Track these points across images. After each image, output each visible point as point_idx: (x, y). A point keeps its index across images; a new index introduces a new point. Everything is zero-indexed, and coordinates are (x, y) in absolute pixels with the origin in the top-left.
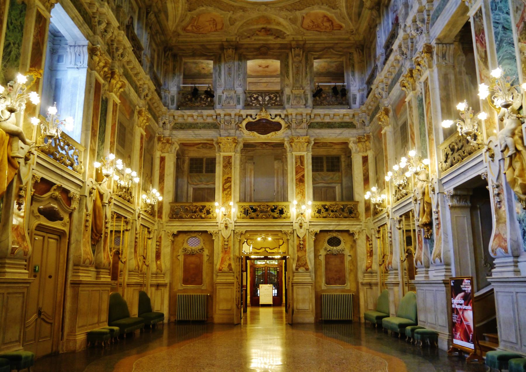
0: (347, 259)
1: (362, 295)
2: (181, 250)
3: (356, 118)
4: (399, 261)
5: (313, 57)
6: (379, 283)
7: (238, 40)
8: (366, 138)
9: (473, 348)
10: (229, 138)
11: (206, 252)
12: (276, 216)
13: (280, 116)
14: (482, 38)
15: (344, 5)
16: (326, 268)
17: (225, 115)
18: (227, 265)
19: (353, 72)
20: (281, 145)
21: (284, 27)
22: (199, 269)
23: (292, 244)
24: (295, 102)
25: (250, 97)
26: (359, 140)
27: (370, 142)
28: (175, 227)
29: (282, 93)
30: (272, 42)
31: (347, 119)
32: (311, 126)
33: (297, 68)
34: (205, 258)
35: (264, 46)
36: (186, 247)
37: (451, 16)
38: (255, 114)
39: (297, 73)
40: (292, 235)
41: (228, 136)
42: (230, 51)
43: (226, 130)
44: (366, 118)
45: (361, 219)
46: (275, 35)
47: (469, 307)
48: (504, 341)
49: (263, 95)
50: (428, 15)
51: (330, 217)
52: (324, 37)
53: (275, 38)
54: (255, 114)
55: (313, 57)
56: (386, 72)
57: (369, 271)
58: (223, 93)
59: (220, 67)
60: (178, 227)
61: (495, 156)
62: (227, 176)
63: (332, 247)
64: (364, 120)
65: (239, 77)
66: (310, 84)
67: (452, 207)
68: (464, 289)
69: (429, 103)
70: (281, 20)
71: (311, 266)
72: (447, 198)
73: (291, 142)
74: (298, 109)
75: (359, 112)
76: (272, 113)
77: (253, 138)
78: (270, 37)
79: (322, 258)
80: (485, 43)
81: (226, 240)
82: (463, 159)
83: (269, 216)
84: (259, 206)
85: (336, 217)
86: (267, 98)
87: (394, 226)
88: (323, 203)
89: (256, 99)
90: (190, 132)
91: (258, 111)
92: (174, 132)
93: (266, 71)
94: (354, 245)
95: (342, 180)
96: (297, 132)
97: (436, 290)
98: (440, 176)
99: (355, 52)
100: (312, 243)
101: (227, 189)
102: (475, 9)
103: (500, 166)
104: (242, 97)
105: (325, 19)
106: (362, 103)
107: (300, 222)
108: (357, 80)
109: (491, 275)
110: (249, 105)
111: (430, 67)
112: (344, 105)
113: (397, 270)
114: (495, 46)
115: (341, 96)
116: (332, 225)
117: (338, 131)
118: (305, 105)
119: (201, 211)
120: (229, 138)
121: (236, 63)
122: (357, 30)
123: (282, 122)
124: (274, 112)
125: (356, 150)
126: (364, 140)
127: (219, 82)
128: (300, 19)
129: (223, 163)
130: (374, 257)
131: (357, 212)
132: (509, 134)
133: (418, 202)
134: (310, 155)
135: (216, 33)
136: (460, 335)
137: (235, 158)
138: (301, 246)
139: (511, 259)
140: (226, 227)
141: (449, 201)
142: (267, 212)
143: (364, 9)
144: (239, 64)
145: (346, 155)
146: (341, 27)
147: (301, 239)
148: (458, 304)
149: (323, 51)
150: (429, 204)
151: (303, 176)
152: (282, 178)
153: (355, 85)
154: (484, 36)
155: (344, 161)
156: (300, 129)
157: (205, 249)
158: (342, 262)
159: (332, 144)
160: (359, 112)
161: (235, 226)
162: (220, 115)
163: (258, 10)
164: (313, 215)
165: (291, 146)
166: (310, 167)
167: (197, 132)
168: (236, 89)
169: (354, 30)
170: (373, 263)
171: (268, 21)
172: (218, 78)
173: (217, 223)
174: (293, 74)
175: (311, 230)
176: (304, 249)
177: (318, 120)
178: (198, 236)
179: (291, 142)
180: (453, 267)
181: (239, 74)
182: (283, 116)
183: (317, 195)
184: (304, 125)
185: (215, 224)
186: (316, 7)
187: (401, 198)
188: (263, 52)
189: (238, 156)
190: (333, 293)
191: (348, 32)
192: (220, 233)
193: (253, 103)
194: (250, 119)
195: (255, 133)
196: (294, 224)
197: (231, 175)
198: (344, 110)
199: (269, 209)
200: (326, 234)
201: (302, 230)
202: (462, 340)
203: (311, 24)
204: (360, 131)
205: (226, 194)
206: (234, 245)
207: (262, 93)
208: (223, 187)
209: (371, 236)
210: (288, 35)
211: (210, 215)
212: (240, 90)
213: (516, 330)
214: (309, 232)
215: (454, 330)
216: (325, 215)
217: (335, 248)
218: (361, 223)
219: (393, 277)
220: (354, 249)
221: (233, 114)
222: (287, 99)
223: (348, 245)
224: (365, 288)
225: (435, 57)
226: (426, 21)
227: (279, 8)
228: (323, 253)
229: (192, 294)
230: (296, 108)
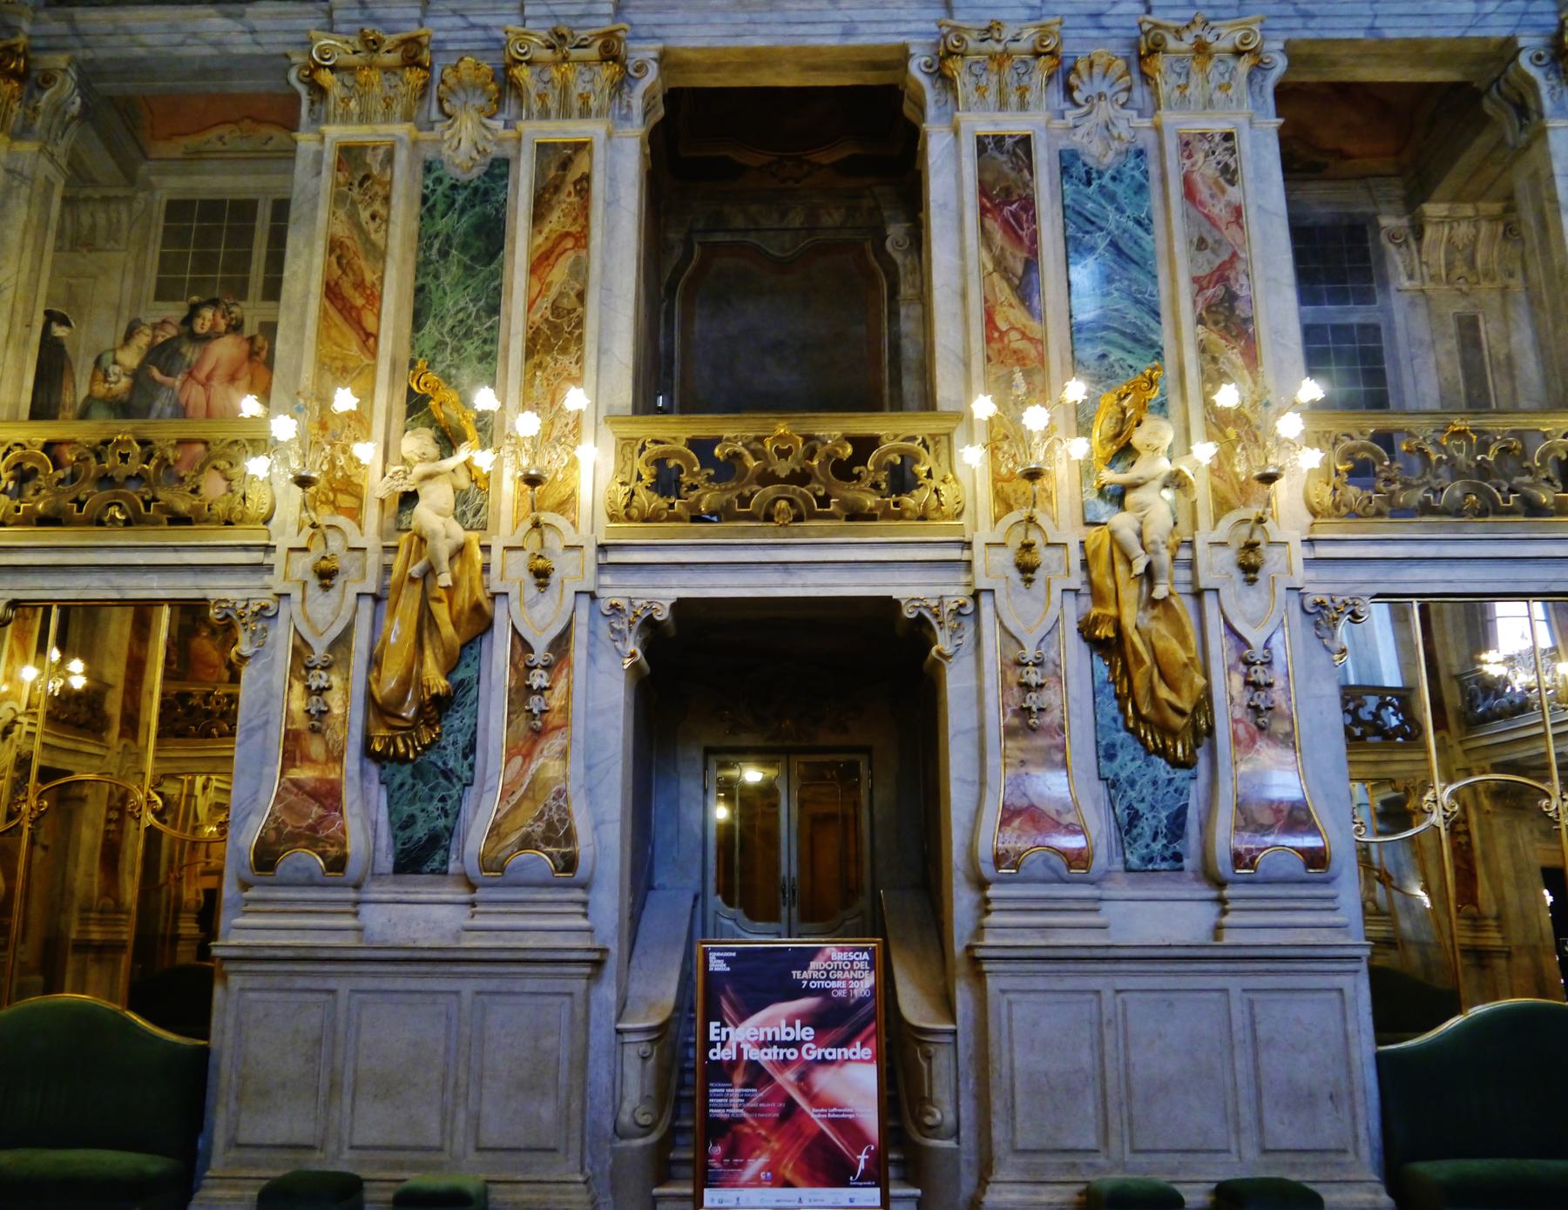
51: (751, 517)
68: (814, 985)
82: (798, 518)
98: (579, 271)
133: (124, 430)
136: (771, 1167)
140: (542, 576)
164: (621, 500)
196: (978, 555)
202: (788, 1184)
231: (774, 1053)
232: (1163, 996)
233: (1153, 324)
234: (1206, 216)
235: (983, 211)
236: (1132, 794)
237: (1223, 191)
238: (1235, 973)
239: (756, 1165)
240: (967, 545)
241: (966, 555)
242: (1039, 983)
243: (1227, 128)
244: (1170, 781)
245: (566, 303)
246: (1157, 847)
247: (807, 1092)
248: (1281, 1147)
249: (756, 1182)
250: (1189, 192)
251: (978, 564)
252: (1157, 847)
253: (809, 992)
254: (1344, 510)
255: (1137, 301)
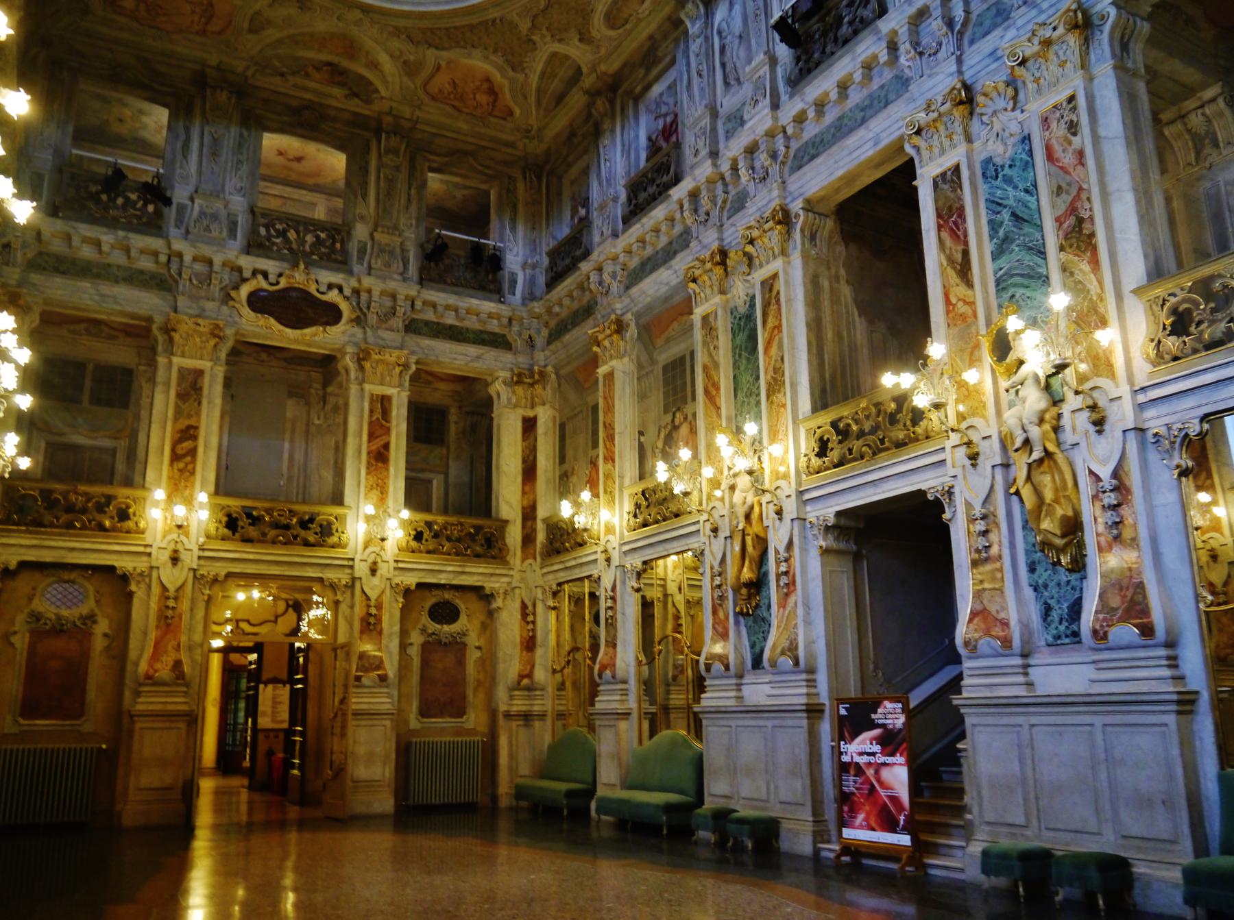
0: (473, 656)
1: (503, 741)
2: (21, 618)
3: (516, 328)
4: (633, 662)
5: (427, 164)
6: (549, 714)
7: (249, 73)
8: (536, 377)
9: (909, 844)
10: (200, 321)
11: (102, 626)
12: (312, 539)
13: (340, 289)
14: (955, 223)
15: (540, 68)
16: (422, 678)
17: (195, 259)
18: (171, 663)
19: (513, 221)
20: (327, 364)
21: (383, 76)
22: (76, 671)
23: (348, 612)
24: (379, 262)
25: (267, 226)
26: (518, 379)
27: (544, 388)
28: (13, 550)
29: (349, 233)
30: (334, 103)
31: (494, 326)
32: (412, 327)
33: (391, 181)
34: (99, 643)
35: (309, 106)
36: (41, 609)
37: (855, 163)
38: (274, 272)
39: (389, 194)
40: (349, 593)
41: (198, 316)
42: (223, 96)
43: (194, 298)
44: (539, 332)
45: (512, 562)
46: (350, 89)
47: (899, 759)
48: (988, 823)
49: (301, 228)
50: (787, 147)
51: (855, 459)
52: (463, 125)
53: (346, 96)
54: (277, 271)
55: (427, 164)
56: (633, 240)
57: (525, 683)
58: (192, 199)
59: (187, 130)
60: (23, 551)
61: (981, 458)
62: (187, 422)
63: (438, 626)
64: (534, 335)
65: (238, 169)
66: (417, 227)
67: (825, 552)
68: (880, 722)
69: (779, 327)
70: (383, 58)
71: (391, 669)
72: (816, 531)
73: (362, 357)
74: (388, 282)
75: (525, 315)
76: (321, 279)
77: (263, 331)
78: (337, 92)
79: (414, 652)
80: (966, 236)
81: (172, 593)
82: (874, 454)
83: (295, 537)
84: (269, 511)
85: (457, 554)
86: (309, 238)
87: (624, 582)
88: (429, 518)
89: (282, 234)
90: (85, 285)
91: (286, 265)
92: (35, 277)
93: (290, 169)
94: (488, 621)
95: (447, 466)
96: (380, 337)
97: (774, 727)
98: (799, 483)
99: (520, 178)
100: (398, 613)
101: (184, 456)
102: (940, 165)
103: (993, 478)
104: (243, 221)
105: (485, 86)
106: (530, 297)
107: (371, 560)
108: (521, 242)
109: (960, 693)
110: (260, 246)
111: (784, 253)
112: (490, 291)
113: (625, 682)
114: (988, 248)
115: (485, 271)
116: (447, 571)
117: (473, 350)
118: (401, 274)
119: (101, 508)
120: (200, 321)
121: (234, 130)
122: (539, 130)
123: (344, 306)
124: (327, 277)
125: (509, 399)
126: (528, 380)
127: (181, 167)
128: (429, 69)
129: (179, 384)
130: (539, 652)
131: (505, 544)
132: (1036, 420)
134: (405, 395)
135: (198, 39)
136: (866, 819)
137: (213, 377)
138: (372, 620)
139: (1018, 661)
141: (821, 538)
142: (287, 527)
143: (574, 90)
144: (241, 135)
145: (460, 407)
146: (511, 113)
147: (373, 603)
148: (861, 754)
149: (453, 157)
150: (762, 542)
151: (386, 446)
152: (303, 445)
153: (515, 252)
154: (965, 221)
155: (456, 423)
156: (387, 329)
157: (99, 618)
158: (461, 662)
159: (430, 379)
160: (525, 315)
161: (199, 558)
162: (180, 255)
163: (338, 18)
164: (404, 544)
165: (362, 368)
166: (404, 426)
167: (106, 288)
168: (227, 197)
169: (535, 127)
170: (537, 667)
171: (351, 48)
172: (179, 156)
173: (146, 546)
174: (378, 194)
175: (397, 580)
176: (378, 627)
177: (430, 316)
178: (80, 580)
179: (362, 357)
180: (822, 678)
181: (239, 162)
182: (347, 292)
183: (416, 496)
184: (397, 322)
185: (141, 549)
186: (478, 53)
187: (657, 522)
188: (307, 121)
189: (221, 371)
190: (438, 739)
191: (518, 130)
192: (154, 574)
193: (274, 244)
194: (261, 283)
195: (272, 321)
197: (199, 421)
198: (492, 304)
199: (295, 520)
200: (427, 593)
201: (375, 581)
202: (873, 829)
203: (448, 88)
204: (522, 360)
205: (180, 471)
206: (192, 610)
207: (298, 222)
208: (173, 450)
209: (534, 606)
210: (382, 98)
211: (130, 524)
212: (238, 203)
213: (1025, 800)
214: (195, 576)
215: (846, 809)
216: (431, 548)
217: (446, 628)
218: (511, 572)
219: (618, 698)
220: (488, 632)
221: (217, 260)
222: (359, 252)
223: (476, 623)
224: (514, 724)
225: (797, 235)
226: (781, 158)
227: (391, 29)
228: (416, 638)
229: (50, 746)
230: (383, 278)
231: (865, 759)
232: (1058, 728)
233: (1040, 261)
234: (1061, 168)
235: (940, 227)
236: (1046, 594)
237: (1070, 143)
238: (1096, 713)
239: (860, 818)
240: (353, 559)
241: (351, 563)
242: (990, 720)
243: (1068, 93)
244: (1068, 582)
245: (778, 365)
246: (1062, 628)
247: (879, 780)
248: (1134, 834)
249: (861, 827)
250: (1050, 156)
251: (356, 567)
252: (1062, 628)
253: (879, 726)
254: (1167, 357)
255: (1030, 249)
